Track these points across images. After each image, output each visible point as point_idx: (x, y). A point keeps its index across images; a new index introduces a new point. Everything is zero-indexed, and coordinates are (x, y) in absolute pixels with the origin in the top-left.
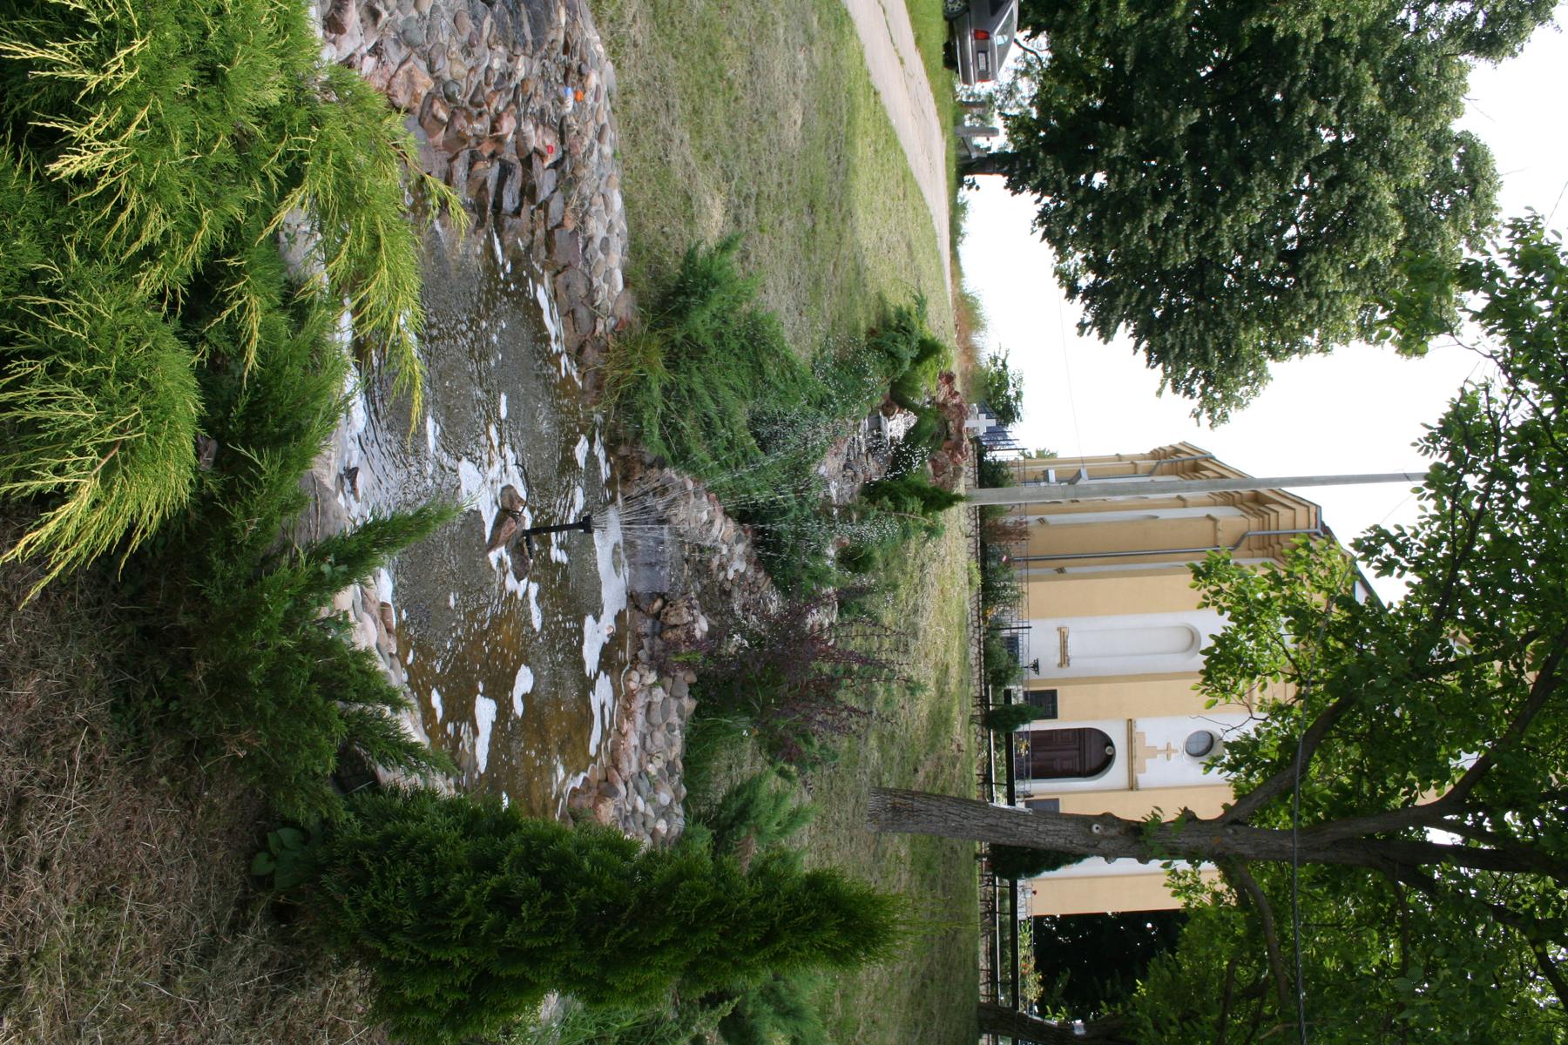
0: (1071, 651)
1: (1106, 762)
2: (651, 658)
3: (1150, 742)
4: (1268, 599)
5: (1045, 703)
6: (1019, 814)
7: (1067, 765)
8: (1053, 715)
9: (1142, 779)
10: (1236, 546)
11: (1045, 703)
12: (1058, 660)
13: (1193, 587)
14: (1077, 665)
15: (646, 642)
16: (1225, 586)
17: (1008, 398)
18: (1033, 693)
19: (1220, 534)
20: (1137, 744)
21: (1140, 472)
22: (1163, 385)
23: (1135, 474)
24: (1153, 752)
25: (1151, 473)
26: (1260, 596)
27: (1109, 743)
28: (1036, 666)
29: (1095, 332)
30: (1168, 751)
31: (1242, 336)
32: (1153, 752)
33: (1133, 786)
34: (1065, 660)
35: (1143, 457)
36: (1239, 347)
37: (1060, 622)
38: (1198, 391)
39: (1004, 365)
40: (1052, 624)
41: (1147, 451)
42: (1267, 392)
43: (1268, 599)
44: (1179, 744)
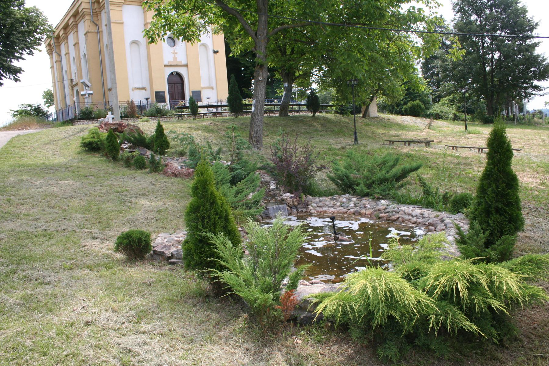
0: (141, 86)
1: (178, 74)
2: (305, 208)
3: (171, 59)
4: (165, 18)
5: (160, 97)
6: (256, 102)
7: (180, 88)
8: (164, 92)
9: (184, 62)
10: (97, 25)
11: (160, 97)
12: (144, 91)
13: (156, 43)
14: (146, 84)
15: (300, 210)
16: (157, 32)
17: (31, 110)
18: (156, 100)
19: (93, 31)
20: (173, 64)
21: (60, 60)
22: (37, 49)
23: (60, 61)
24: (175, 58)
25: (60, 55)
26: (163, 21)
27: (172, 73)
28: (147, 99)
29: (18, 75)
30: (174, 53)
31: (19, 16)
32: (175, 58)
33: (187, 66)
34: (144, 89)
35: (52, 58)
36: (23, 18)
37: (131, 90)
38: (39, 35)
39: (17, 111)
40: (131, 93)
41: (48, 57)
42: (41, 8)
43: (165, 18)
44: (171, 49)
